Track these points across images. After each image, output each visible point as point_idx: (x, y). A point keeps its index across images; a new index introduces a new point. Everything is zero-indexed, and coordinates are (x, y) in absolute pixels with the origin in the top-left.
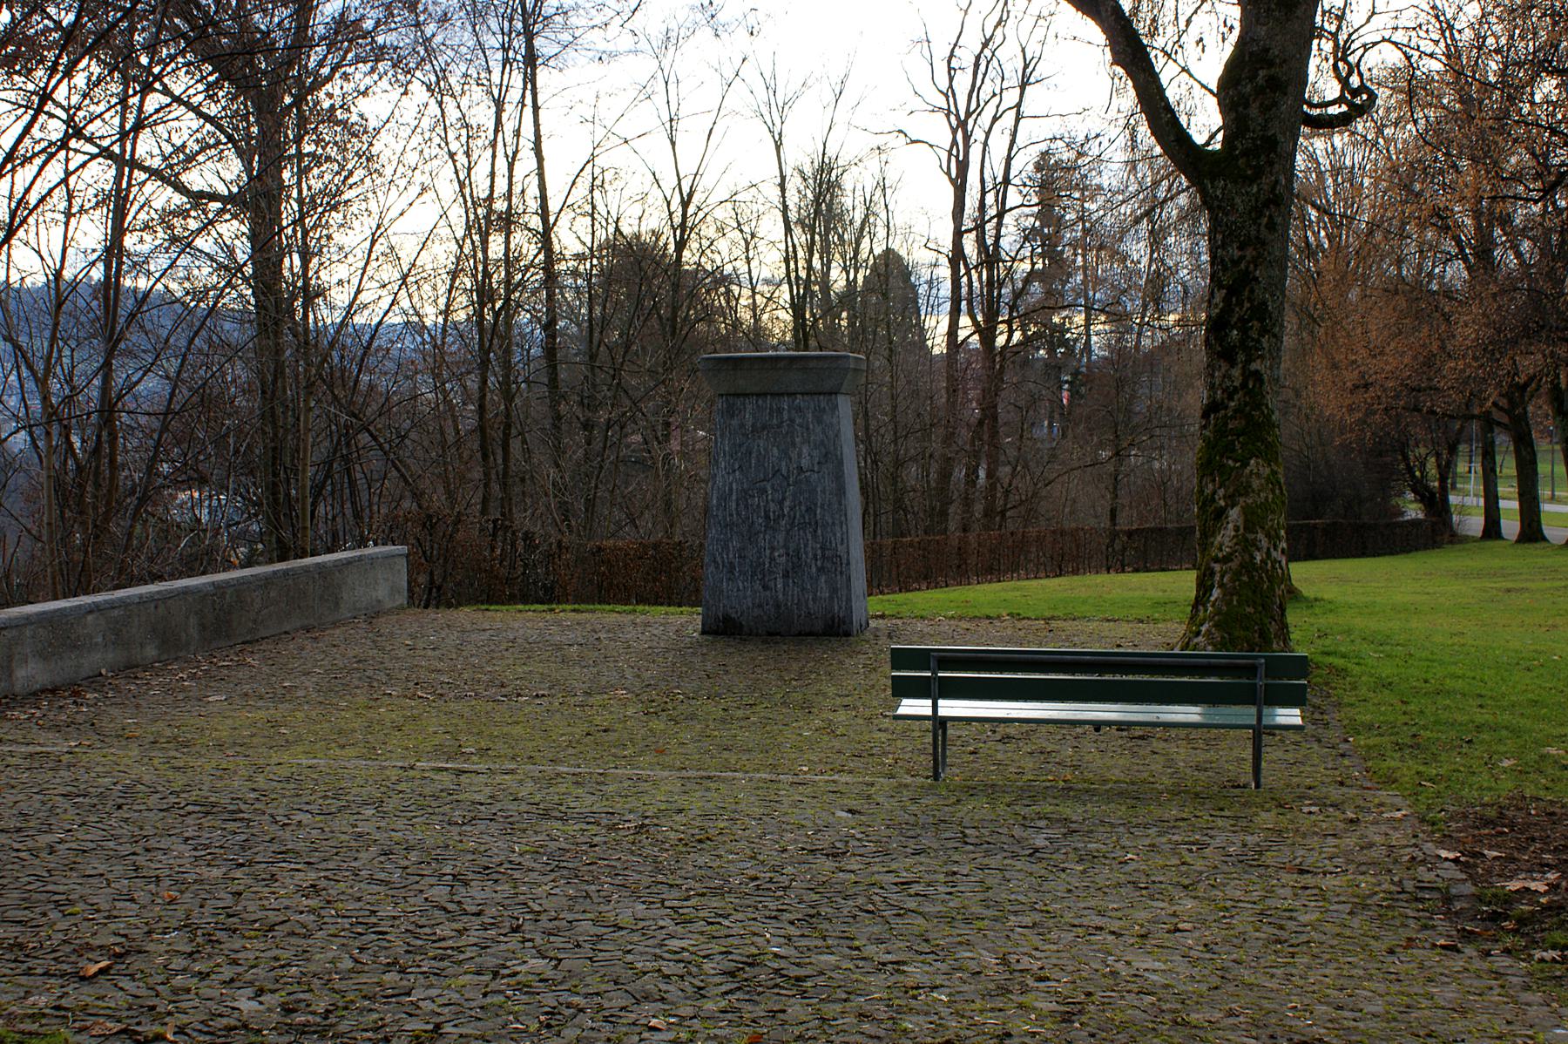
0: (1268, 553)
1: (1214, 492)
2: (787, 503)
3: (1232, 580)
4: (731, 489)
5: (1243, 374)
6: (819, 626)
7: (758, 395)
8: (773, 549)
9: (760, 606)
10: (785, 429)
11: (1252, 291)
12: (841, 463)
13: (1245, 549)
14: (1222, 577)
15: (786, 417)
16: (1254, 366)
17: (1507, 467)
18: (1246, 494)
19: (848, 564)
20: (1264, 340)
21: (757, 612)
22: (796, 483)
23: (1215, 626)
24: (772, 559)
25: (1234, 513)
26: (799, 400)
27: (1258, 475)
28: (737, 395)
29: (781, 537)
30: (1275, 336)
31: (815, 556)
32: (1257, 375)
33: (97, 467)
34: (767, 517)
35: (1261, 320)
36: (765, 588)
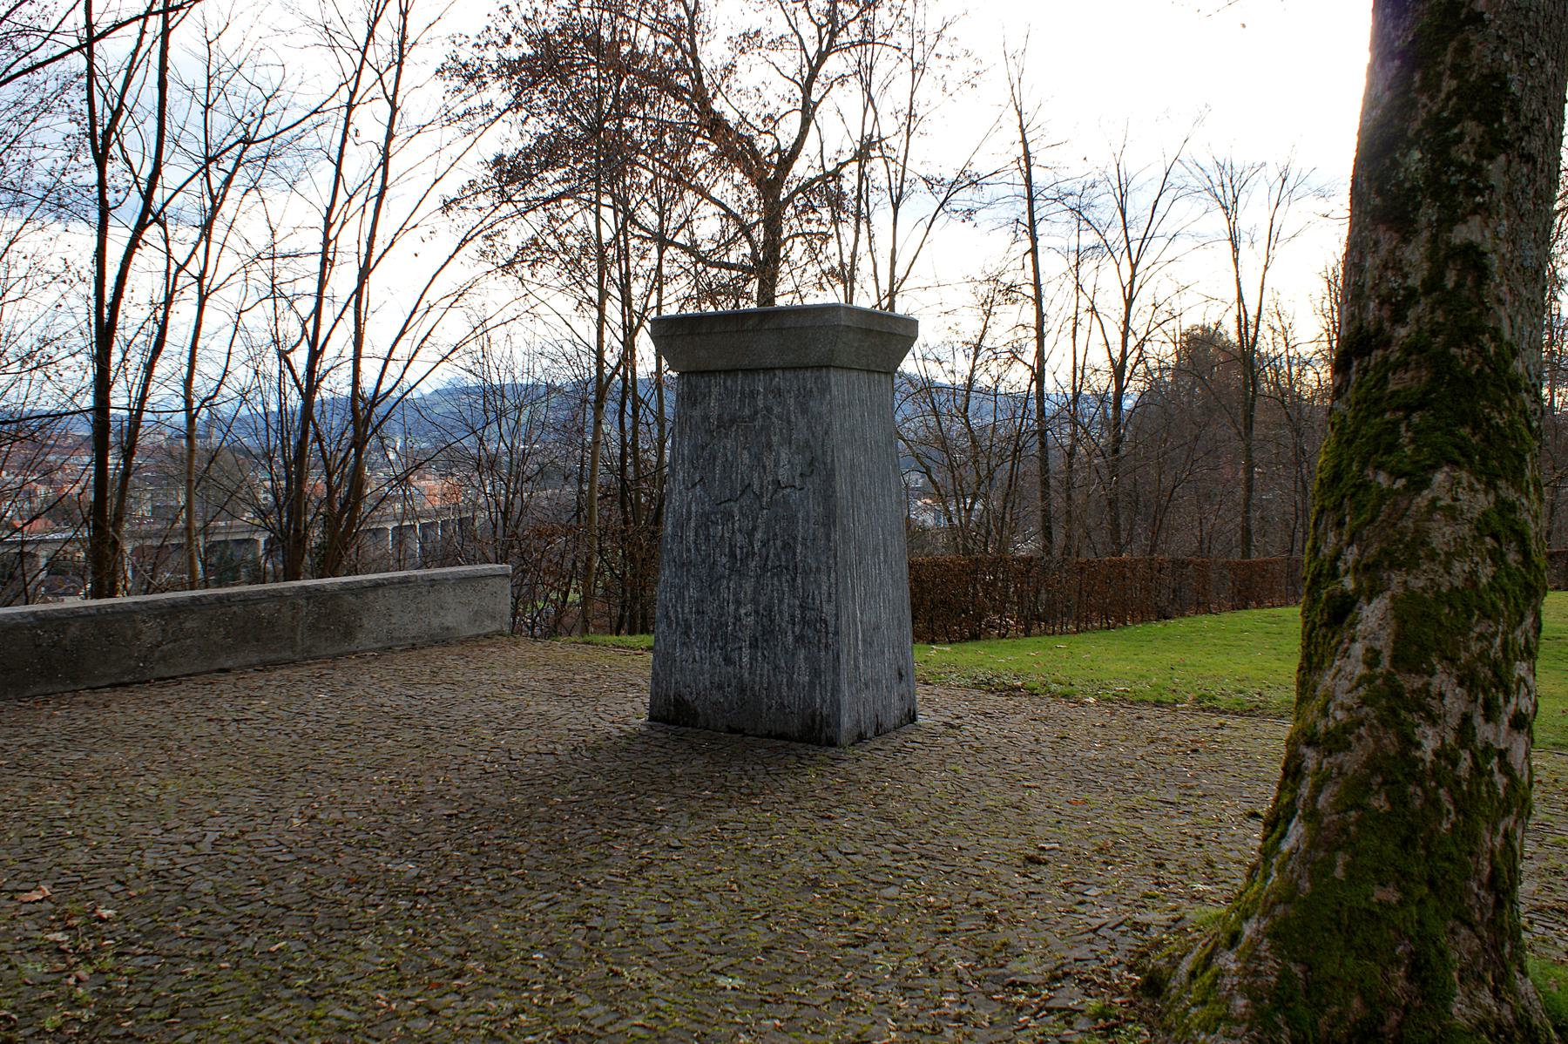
0: (1465, 728)
1: (1338, 556)
2: (759, 535)
3: (1342, 807)
4: (689, 512)
5: (1431, 258)
6: (795, 725)
7: (727, 372)
8: (738, 603)
9: (720, 687)
10: (758, 423)
11: (1465, 49)
12: (831, 475)
13: (1390, 719)
14: (1317, 789)
15: (760, 404)
16: (1462, 234)
17: (120, 398)
18: (1411, 564)
19: (836, 633)
20: (1495, 170)
21: (717, 696)
22: (772, 503)
23: (1274, 935)
24: (738, 619)
25: (1372, 615)
26: (779, 379)
27: (1452, 514)
28: (702, 373)
29: (749, 586)
30: (1528, 158)
31: (793, 616)
32: (1472, 258)
33: (1012, 479)
34: (733, 555)
35: (1489, 116)
36: (728, 660)
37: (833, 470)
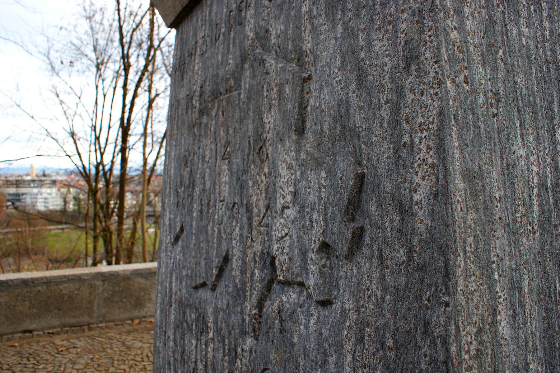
37: (441, 245)
